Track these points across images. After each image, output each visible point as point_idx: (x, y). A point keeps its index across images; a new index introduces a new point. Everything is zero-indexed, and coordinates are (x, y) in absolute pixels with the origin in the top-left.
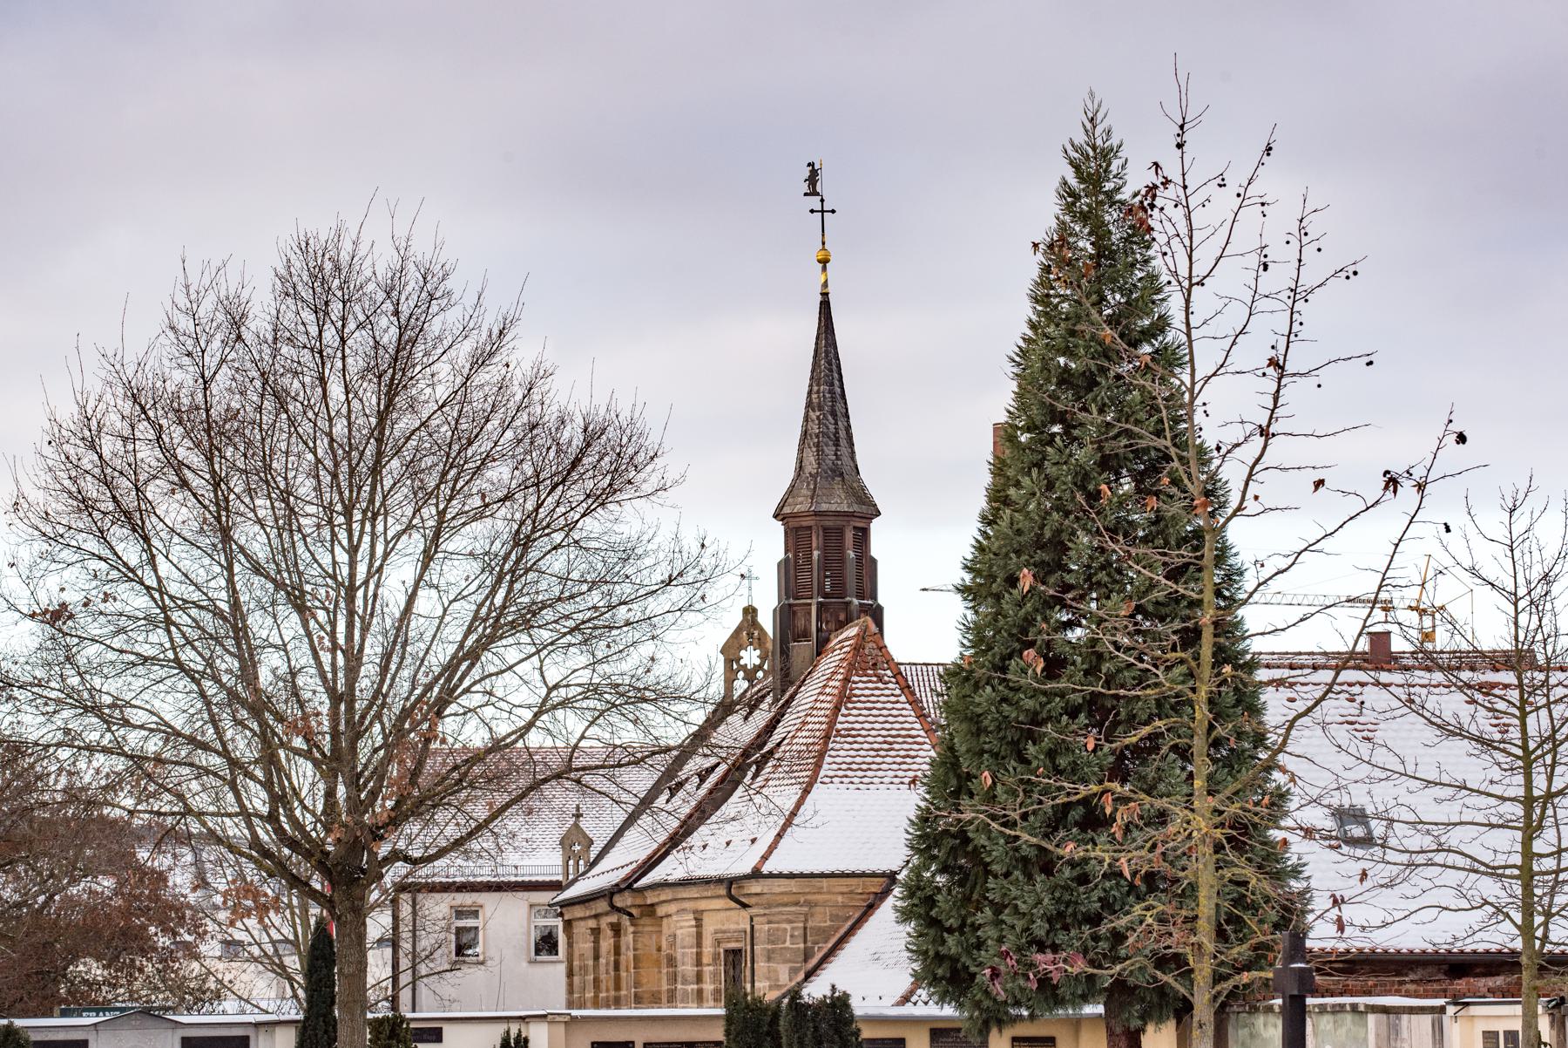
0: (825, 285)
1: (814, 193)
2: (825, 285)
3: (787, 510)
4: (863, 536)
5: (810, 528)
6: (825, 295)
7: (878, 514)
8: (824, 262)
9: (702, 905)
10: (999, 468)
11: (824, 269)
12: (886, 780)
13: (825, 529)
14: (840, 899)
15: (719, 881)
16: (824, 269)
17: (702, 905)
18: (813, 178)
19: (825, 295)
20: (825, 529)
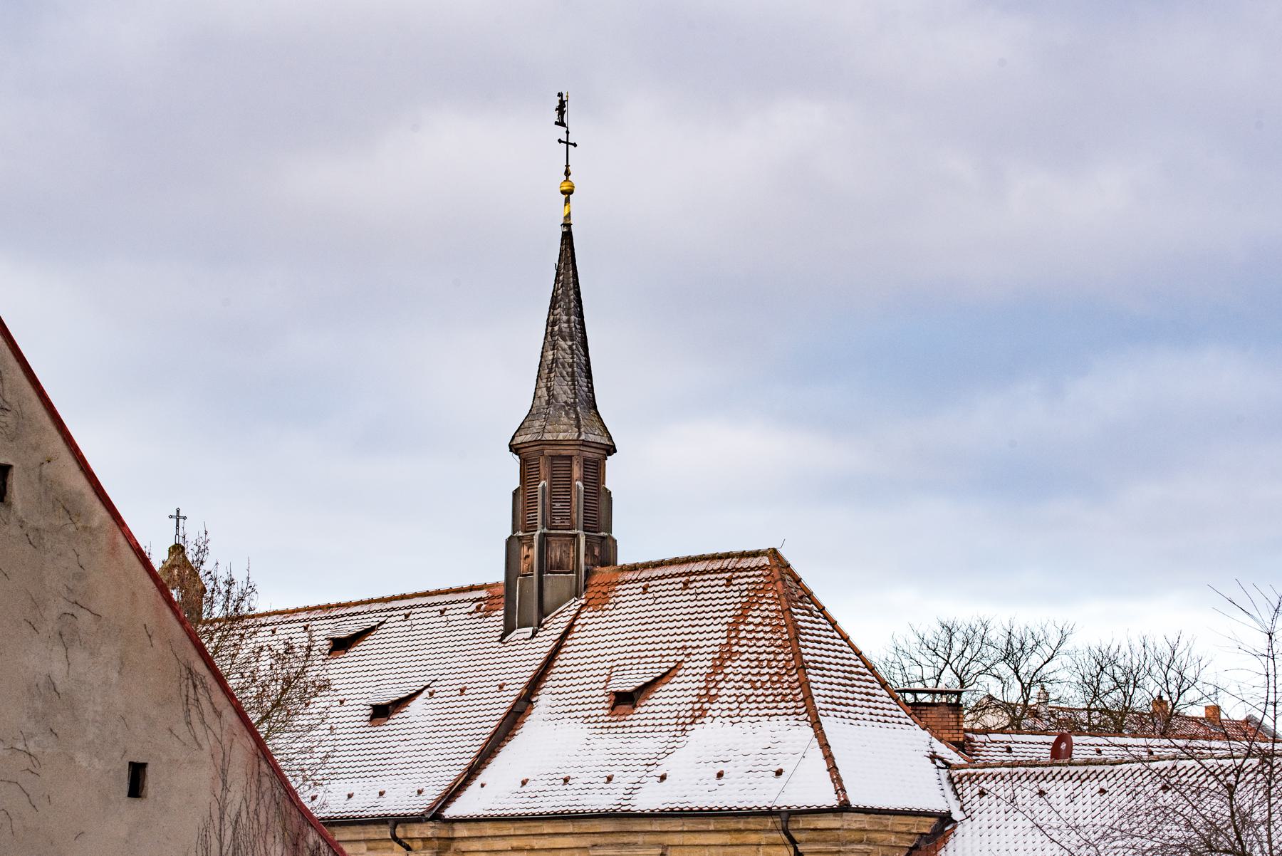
0: (568, 216)
1: (561, 123)
2: (568, 216)
3: (519, 440)
4: (595, 472)
5: (570, 457)
6: (567, 225)
7: (615, 451)
8: (568, 193)
9: (667, 839)
10: (8, 490)
11: (567, 201)
12: (865, 716)
13: (585, 460)
14: (893, 838)
15: (770, 813)
16: (567, 201)
17: (667, 839)
18: (561, 109)
19: (567, 225)
20: (585, 460)
